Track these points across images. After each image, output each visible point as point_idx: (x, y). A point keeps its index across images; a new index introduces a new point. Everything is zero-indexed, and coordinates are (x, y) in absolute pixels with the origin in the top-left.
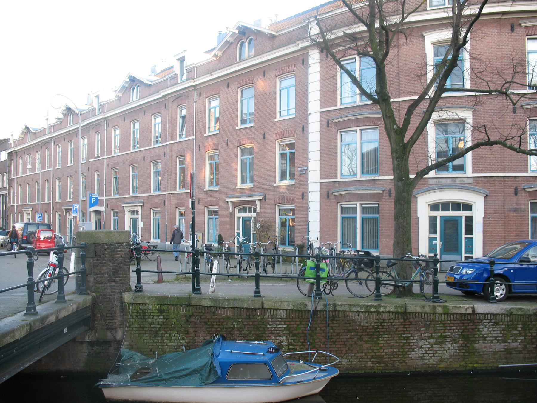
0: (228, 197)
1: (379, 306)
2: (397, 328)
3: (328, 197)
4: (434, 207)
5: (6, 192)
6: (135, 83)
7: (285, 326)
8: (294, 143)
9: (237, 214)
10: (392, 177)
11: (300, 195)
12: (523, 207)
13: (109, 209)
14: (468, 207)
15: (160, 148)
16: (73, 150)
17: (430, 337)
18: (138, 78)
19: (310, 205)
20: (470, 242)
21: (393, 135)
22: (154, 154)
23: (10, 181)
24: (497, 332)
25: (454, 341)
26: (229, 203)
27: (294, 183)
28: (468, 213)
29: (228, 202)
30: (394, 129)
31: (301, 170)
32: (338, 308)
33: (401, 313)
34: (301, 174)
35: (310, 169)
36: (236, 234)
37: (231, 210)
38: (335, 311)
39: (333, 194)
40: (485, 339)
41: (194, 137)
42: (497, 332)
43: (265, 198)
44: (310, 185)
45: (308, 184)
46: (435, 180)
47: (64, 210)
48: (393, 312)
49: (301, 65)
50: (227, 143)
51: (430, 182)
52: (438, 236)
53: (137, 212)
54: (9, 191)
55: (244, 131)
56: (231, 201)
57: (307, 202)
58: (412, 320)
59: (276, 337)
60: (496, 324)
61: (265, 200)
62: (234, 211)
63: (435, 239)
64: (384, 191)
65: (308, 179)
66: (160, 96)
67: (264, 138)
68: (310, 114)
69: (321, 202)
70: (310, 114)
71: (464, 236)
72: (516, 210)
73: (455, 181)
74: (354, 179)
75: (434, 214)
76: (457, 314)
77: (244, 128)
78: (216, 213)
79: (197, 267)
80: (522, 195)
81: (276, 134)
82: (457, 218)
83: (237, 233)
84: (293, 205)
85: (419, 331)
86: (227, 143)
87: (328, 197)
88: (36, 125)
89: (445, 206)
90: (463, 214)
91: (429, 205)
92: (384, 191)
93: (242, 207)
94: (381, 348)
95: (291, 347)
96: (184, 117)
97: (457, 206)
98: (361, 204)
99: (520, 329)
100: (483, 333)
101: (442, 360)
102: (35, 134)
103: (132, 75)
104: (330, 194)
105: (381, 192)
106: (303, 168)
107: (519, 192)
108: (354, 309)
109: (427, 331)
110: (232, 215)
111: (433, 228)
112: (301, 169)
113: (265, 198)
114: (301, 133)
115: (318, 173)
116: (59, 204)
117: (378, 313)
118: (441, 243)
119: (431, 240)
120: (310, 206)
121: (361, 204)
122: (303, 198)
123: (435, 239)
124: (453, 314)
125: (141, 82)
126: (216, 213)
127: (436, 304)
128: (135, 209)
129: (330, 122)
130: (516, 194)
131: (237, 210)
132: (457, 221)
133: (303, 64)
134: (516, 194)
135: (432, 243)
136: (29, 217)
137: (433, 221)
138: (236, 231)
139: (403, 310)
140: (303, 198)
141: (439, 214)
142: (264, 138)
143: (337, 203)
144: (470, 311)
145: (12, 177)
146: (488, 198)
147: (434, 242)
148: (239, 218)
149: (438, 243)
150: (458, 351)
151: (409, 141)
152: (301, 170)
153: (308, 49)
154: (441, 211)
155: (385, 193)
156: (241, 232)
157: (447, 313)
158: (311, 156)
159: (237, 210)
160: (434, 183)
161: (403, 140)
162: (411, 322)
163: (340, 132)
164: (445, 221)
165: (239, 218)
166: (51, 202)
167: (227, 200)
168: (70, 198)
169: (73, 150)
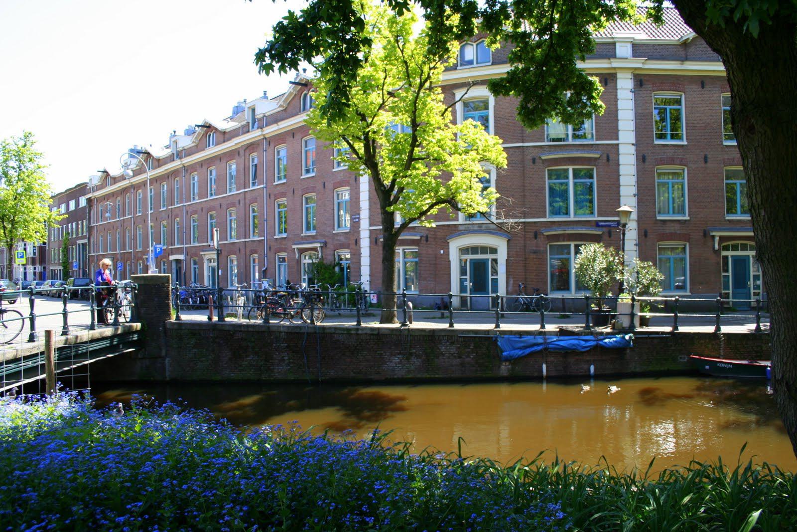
0: (295, 244)
2: (372, 347)
3: (376, 243)
4: (464, 251)
5: (86, 241)
6: (211, 129)
7: (286, 345)
10: (381, 227)
11: (354, 241)
12: (542, 249)
13: (189, 257)
14: (494, 251)
16: (165, 193)
17: (399, 354)
18: (213, 125)
20: (495, 282)
22: (229, 202)
23: (90, 229)
24: (453, 350)
25: (418, 356)
27: (315, 234)
28: (493, 256)
33: (375, 335)
37: (297, 256)
38: (324, 333)
40: (443, 355)
41: (265, 185)
42: (453, 350)
43: (325, 244)
46: (465, 226)
51: (461, 228)
52: (468, 277)
54: (89, 239)
57: (360, 248)
58: (384, 340)
60: (452, 343)
61: (326, 246)
63: (466, 280)
66: (233, 144)
69: (371, 247)
72: (535, 252)
73: (481, 227)
75: (464, 257)
77: (307, 178)
79: (221, 301)
80: (541, 240)
88: (262, 48)
89: (474, 250)
90: (490, 257)
91: (460, 249)
92: (421, 237)
94: (360, 362)
95: (291, 361)
96: (256, 166)
97: (484, 250)
99: (472, 347)
100: (442, 350)
101: (409, 372)
102: (115, 180)
103: (207, 121)
107: (538, 236)
111: (463, 272)
113: (325, 244)
114: (354, 183)
117: (357, 334)
118: (471, 284)
119: (462, 281)
121: (404, 249)
122: (356, 245)
123: (466, 280)
125: (216, 129)
130: (536, 237)
132: (474, 263)
134: (536, 237)
140: (356, 245)
145: (93, 225)
146: (511, 242)
147: (465, 283)
149: (469, 284)
154: (490, 253)
160: (463, 229)
162: (383, 342)
166: (725, 181)
168: (140, 247)
169: (165, 193)
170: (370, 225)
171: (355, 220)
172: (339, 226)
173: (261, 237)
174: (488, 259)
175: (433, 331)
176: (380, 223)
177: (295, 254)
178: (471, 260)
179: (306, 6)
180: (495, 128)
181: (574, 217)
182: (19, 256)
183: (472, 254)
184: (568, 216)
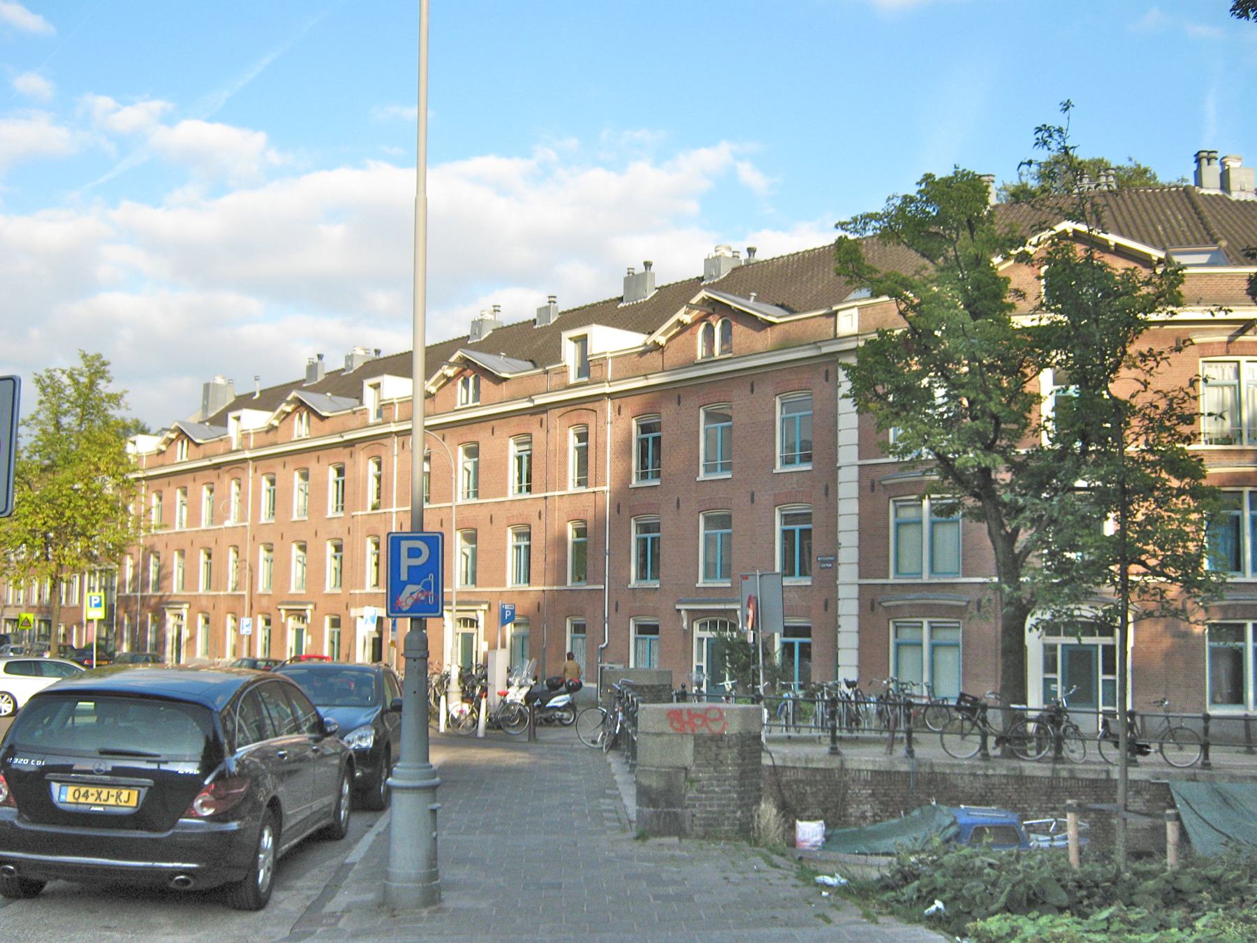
0: (680, 602)
1: (987, 768)
3: (872, 608)
8: (810, 514)
9: (697, 633)
11: (822, 603)
15: (528, 502)
19: (841, 621)
21: (1000, 544)
26: (683, 612)
29: (679, 611)
30: (1001, 535)
31: (822, 562)
32: (937, 769)
34: (822, 568)
35: (841, 560)
36: (694, 669)
37: (685, 624)
38: (933, 772)
39: (883, 604)
44: (840, 587)
45: (836, 586)
47: (283, 612)
48: (1004, 776)
49: (823, 380)
50: (678, 503)
52: (1059, 676)
53: (473, 623)
55: (713, 485)
56: (686, 610)
58: (1029, 786)
59: (858, 805)
60: (1138, 793)
62: (691, 626)
63: (1055, 681)
64: (968, 602)
65: (836, 578)
67: (752, 502)
68: (840, 468)
69: (861, 616)
70: (840, 468)
71: (1101, 677)
74: (919, 581)
75: (1052, 640)
76: (1086, 779)
78: (654, 630)
81: (775, 495)
82: (1090, 649)
83: (1113, 673)
84: (808, 620)
85: (1039, 800)
86: (678, 503)
87: (872, 608)
93: (708, 620)
98: (930, 623)
104: (876, 604)
105: (964, 604)
106: (828, 558)
108: (957, 770)
109: (1049, 800)
110: (688, 634)
111: (1050, 666)
112: (824, 559)
114: (823, 497)
115: (855, 568)
116: (266, 598)
117: (986, 776)
119: (1047, 682)
120: (840, 623)
124: (1082, 780)
126: (654, 630)
127: (1058, 766)
128: (472, 615)
129: (876, 483)
131: (696, 626)
132: (1090, 653)
133: (827, 380)
135: (1049, 687)
136: (180, 622)
137: (1049, 650)
138: (695, 663)
139: (1018, 772)
141: (1060, 640)
142: (752, 502)
143: (889, 620)
144: (1103, 776)
147: (1054, 686)
148: (701, 640)
149: (1059, 687)
150: (1048, 360)
151: (1021, 552)
152: (822, 562)
153: (837, 355)
155: (971, 604)
156: (704, 664)
157: (1073, 778)
158: (842, 538)
159: (696, 626)
161: (1013, 550)
162: (1028, 789)
163: (894, 501)
164: (1070, 651)
165: (701, 640)
167: (678, 607)
170: (860, 577)
171: (823, 565)
172: (897, 571)
173: (598, 584)
174: (1096, 646)
175: (11, 850)
176: (994, 571)
177: (680, 620)
178: (1063, 645)
179: (944, 176)
180: (284, 385)
181: (895, 578)
182: (94, 603)
183: (1065, 634)
184: (1240, 574)
